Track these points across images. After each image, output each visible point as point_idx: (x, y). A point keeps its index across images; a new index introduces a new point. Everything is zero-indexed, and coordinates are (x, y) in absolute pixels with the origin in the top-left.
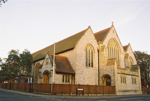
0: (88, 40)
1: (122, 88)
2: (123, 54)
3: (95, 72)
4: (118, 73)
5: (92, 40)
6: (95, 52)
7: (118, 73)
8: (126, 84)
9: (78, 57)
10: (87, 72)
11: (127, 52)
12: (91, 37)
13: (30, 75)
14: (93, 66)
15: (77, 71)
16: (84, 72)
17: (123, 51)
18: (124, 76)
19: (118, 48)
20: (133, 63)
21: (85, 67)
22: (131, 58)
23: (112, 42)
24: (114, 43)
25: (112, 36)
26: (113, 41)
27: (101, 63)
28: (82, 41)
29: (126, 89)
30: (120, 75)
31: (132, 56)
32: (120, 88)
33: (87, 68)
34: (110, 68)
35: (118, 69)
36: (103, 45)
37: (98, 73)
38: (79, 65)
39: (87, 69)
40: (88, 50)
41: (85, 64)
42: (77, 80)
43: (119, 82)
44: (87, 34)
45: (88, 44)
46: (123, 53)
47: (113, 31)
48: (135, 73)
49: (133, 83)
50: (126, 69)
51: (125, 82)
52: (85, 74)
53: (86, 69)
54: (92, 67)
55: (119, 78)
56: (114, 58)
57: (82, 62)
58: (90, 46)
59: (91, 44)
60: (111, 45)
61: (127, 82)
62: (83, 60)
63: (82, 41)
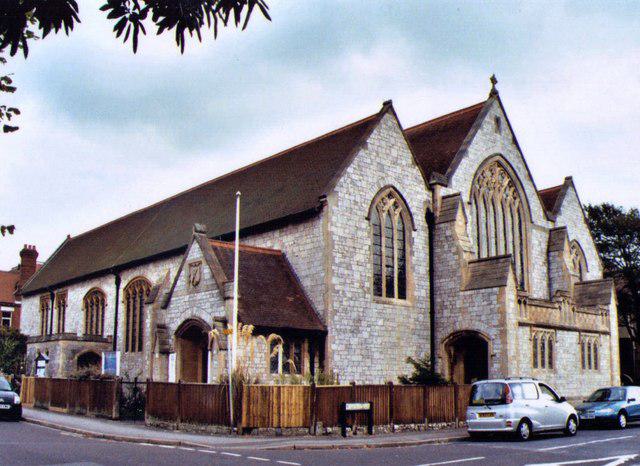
0: (381, 167)
5: (398, 170)
8: (555, 372)
12: (394, 153)
14: (409, 293)
15: (336, 318)
16: (364, 323)
22: (576, 245)
30: (529, 332)
33: (378, 302)
35: (523, 305)
39: (380, 306)
49: (584, 367)
52: (369, 329)
54: (402, 295)
57: (357, 276)
58: (390, 196)
61: (558, 364)
62: (361, 268)
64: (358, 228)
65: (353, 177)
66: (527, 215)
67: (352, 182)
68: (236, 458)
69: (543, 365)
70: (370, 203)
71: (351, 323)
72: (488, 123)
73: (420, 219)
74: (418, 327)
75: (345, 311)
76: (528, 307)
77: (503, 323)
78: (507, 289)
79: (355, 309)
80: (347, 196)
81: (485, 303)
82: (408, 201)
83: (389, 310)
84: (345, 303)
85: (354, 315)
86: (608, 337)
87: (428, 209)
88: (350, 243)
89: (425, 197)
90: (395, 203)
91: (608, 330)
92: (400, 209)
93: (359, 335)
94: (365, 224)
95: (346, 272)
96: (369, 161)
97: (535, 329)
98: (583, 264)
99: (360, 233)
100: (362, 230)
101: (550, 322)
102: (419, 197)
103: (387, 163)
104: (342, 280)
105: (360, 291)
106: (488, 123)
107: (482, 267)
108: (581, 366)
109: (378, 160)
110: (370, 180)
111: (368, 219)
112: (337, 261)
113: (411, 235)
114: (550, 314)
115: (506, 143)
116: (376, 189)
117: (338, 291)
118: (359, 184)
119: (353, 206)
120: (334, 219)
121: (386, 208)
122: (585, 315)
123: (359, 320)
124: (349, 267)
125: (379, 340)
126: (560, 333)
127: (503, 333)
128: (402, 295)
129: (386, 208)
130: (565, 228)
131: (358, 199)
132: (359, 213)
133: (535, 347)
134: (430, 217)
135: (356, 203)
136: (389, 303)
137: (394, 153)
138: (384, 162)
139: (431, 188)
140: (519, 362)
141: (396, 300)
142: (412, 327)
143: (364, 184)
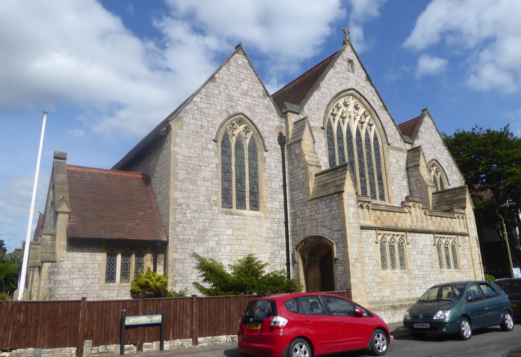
0: (230, 98)
1: (387, 292)
2: (400, 149)
3: (270, 229)
4: (363, 228)
5: (249, 100)
6: (267, 148)
7: (363, 228)
8: (409, 273)
9: (181, 172)
10: (229, 232)
11: (417, 143)
12: (244, 86)
13: (126, 255)
14: (261, 205)
15: (178, 229)
16: (210, 233)
17: (398, 137)
18: (451, 241)
19: (374, 127)
20: (445, 181)
21: (218, 208)
22: (435, 163)
23: (346, 105)
24: (356, 108)
25: (343, 81)
26: (352, 102)
27: (435, 218)
28: (204, 105)
29: (407, 296)
30: (374, 236)
31: (439, 156)
32: (375, 294)
33: (227, 213)
34: (328, 210)
35: (366, 210)
36: (302, 117)
37: (284, 233)
38: (187, 205)
39: (228, 217)
40: (233, 141)
41: (218, 198)
42: (179, 266)
43: (371, 268)
44: (226, 77)
45: (231, 117)
46: (396, 145)
47: (350, 61)
48: (450, 223)
49: (441, 266)
50: (406, 210)
51: (455, 262)
52: (216, 239)
53: (223, 219)
54: (255, 206)
55: (371, 249)
56: (338, 164)
57: (203, 190)
58: (240, 122)
59: (248, 115)
60: (344, 118)
61: (410, 265)
62: (206, 183)
63: (204, 105)
64: (205, 149)
65: (200, 105)
66: (446, 182)
67: (200, 110)
68: (518, 238)
69: (393, 266)
70: (217, 127)
71: (196, 233)
72: (341, 64)
73: (272, 142)
74: (272, 236)
75: (189, 222)
76: (372, 212)
77: (342, 230)
78: (345, 195)
79: (201, 220)
80: (193, 121)
81: (328, 210)
82: (259, 126)
83: (237, 220)
84: (188, 215)
85: (200, 226)
86: (467, 237)
87: (281, 134)
88: (195, 161)
89: (277, 123)
90: (246, 128)
91: (466, 232)
92: (251, 133)
93: (204, 244)
94: (212, 145)
95: (191, 187)
96: (216, 92)
97: (437, 235)
98: (444, 179)
99: (206, 153)
100: (210, 150)
101: (399, 226)
102: (271, 123)
103: (236, 94)
104: (185, 194)
105: (207, 203)
106: (341, 64)
107: (324, 178)
108: (438, 266)
109: (227, 91)
110: (219, 108)
111: (215, 141)
112: (180, 177)
113: (262, 155)
114: (398, 218)
115: (359, 80)
116: (225, 116)
117: (181, 205)
118: (206, 111)
119: (198, 130)
120: (178, 140)
121: (236, 132)
122: (439, 218)
123: (206, 231)
124: (193, 182)
125: (228, 248)
126: (410, 236)
127: (344, 237)
128: (255, 206)
129: (236, 132)
130: (419, 147)
131: (205, 124)
132: (205, 135)
133: (382, 249)
134: (282, 140)
135: (202, 127)
136: (238, 215)
137: (244, 86)
138: (233, 93)
139: (283, 115)
140: (364, 264)
141: (248, 212)
142: (265, 235)
143: (212, 111)
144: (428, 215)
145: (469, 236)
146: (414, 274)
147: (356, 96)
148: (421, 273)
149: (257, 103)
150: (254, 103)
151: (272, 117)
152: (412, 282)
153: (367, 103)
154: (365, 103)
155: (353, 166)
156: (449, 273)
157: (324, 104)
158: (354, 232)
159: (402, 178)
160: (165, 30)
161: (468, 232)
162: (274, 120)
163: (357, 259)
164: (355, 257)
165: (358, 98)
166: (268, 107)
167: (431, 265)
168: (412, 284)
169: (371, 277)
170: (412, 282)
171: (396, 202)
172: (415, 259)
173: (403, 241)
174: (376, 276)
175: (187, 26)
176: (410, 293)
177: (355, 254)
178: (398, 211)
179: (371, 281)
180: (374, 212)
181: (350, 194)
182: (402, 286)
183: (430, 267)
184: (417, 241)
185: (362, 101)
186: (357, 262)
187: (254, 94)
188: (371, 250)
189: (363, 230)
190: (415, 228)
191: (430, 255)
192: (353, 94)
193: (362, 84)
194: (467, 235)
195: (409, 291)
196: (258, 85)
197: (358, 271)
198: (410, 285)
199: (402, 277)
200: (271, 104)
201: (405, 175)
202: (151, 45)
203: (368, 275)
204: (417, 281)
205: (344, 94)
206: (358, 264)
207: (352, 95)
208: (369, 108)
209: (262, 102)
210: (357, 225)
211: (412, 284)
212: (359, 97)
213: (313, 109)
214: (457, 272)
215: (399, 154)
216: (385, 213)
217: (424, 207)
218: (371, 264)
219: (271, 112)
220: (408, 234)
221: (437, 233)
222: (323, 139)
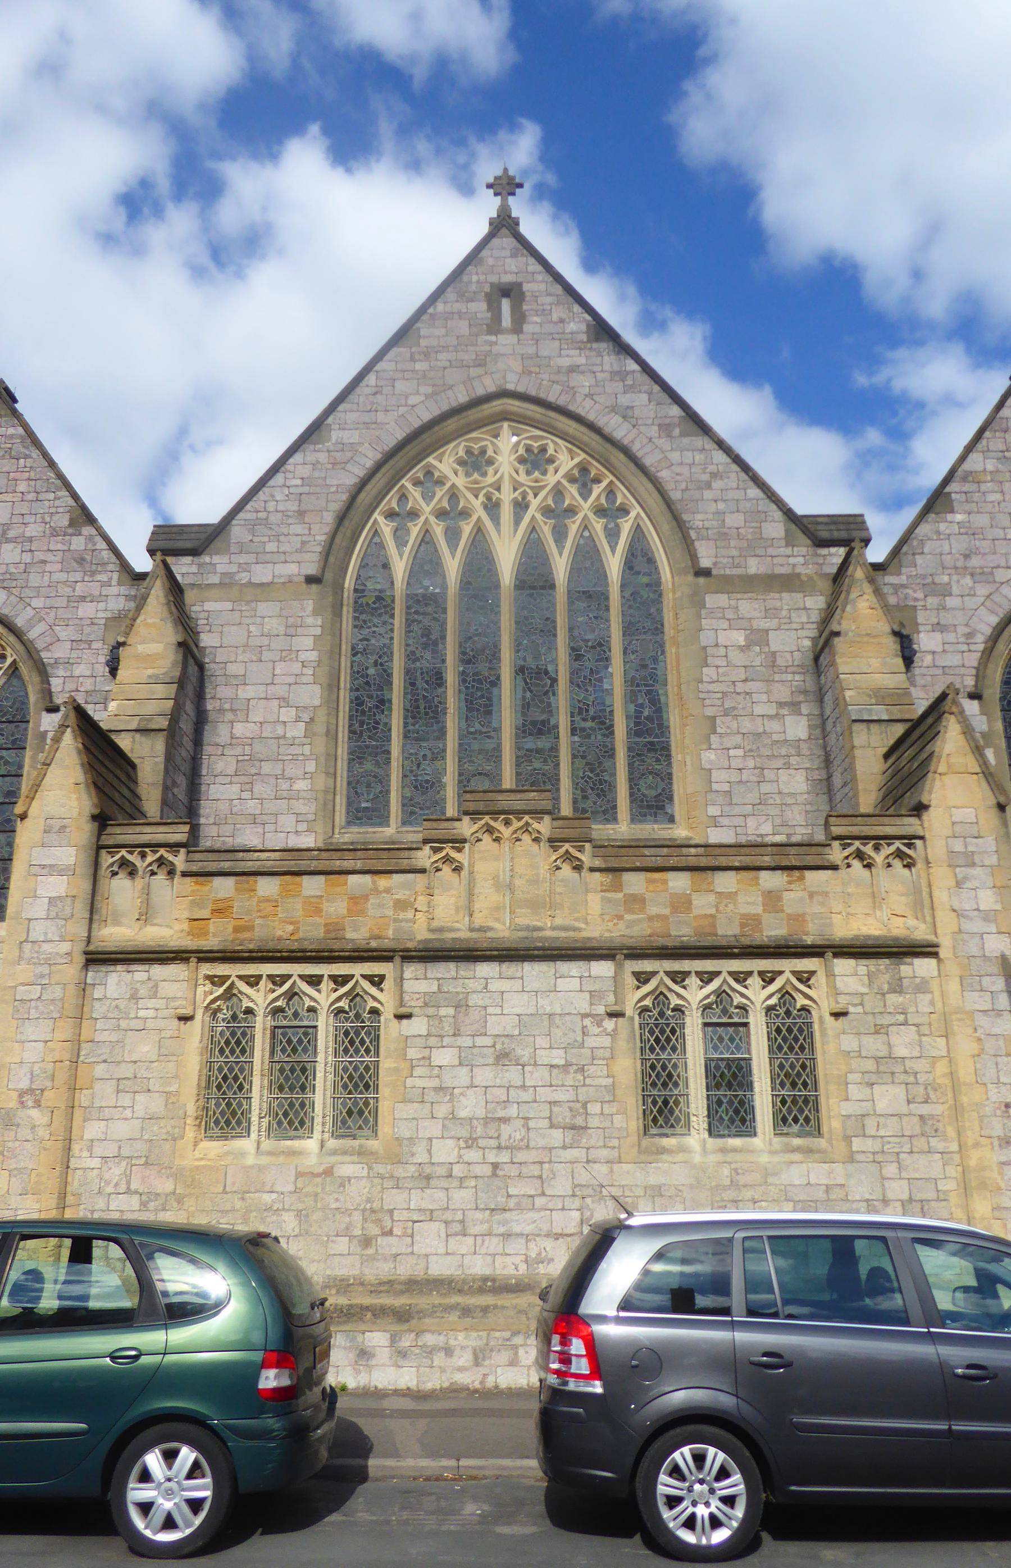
144: (592, 870)
145: (935, 955)
146: (421, 1157)
147: (525, 417)
148: (472, 1155)
149: (39, 556)
150: (27, 558)
151: (95, 589)
152: (395, 1199)
153: (583, 429)
154: (571, 431)
155: (489, 699)
156: (719, 1157)
157: (333, 489)
158: (42, 976)
159: (781, 705)
160: (898, 385)
161: (936, 934)
162: (103, 598)
163: (31, 1091)
164: (25, 1084)
165: (538, 421)
166: (83, 559)
167: (562, 1115)
168: (391, 1212)
169: (116, 1171)
170: (395, 1199)
171: (725, 821)
172: (440, 1089)
173: (807, 1002)
174: (146, 1164)
175: (958, 349)
176: (370, 1251)
177: (26, 1069)
178: (359, 865)
179: (110, 1189)
180: (196, 883)
181: (57, 824)
182: (316, 1216)
183: (552, 1126)
184: (474, 1000)
185: (560, 425)
186: (30, 1103)
187: (31, 531)
188: (146, 1049)
189: (112, 968)
190: (468, 940)
191: (568, 1065)
192: (506, 412)
193: (565, 362)
194: (927, 950)
195: (367, 1242)
196: (51, 496)
197: (28, 1145)
198: (371, 1213)
199: (328, 1172)
200: (98, 547)
201: (805, 692)
202: (874, 437)
203: (96, 1163)
204: (441, 1195)
205: (452, 424)
206: (34, 1113)
207: (505, 416)
208: (594, 444)
209: (60, 547)
210: (65, 947)
211: (391, 1212)
212: (538, 416)
213: (274, 518)
214: (797, 1157)
215: (770, 604)
216: (267, 886)
217: (559, 834)
218: (128, 1113)
219: (93, 573)
220: (411, 970)
221: (636, 953)
222: (310, 620)
